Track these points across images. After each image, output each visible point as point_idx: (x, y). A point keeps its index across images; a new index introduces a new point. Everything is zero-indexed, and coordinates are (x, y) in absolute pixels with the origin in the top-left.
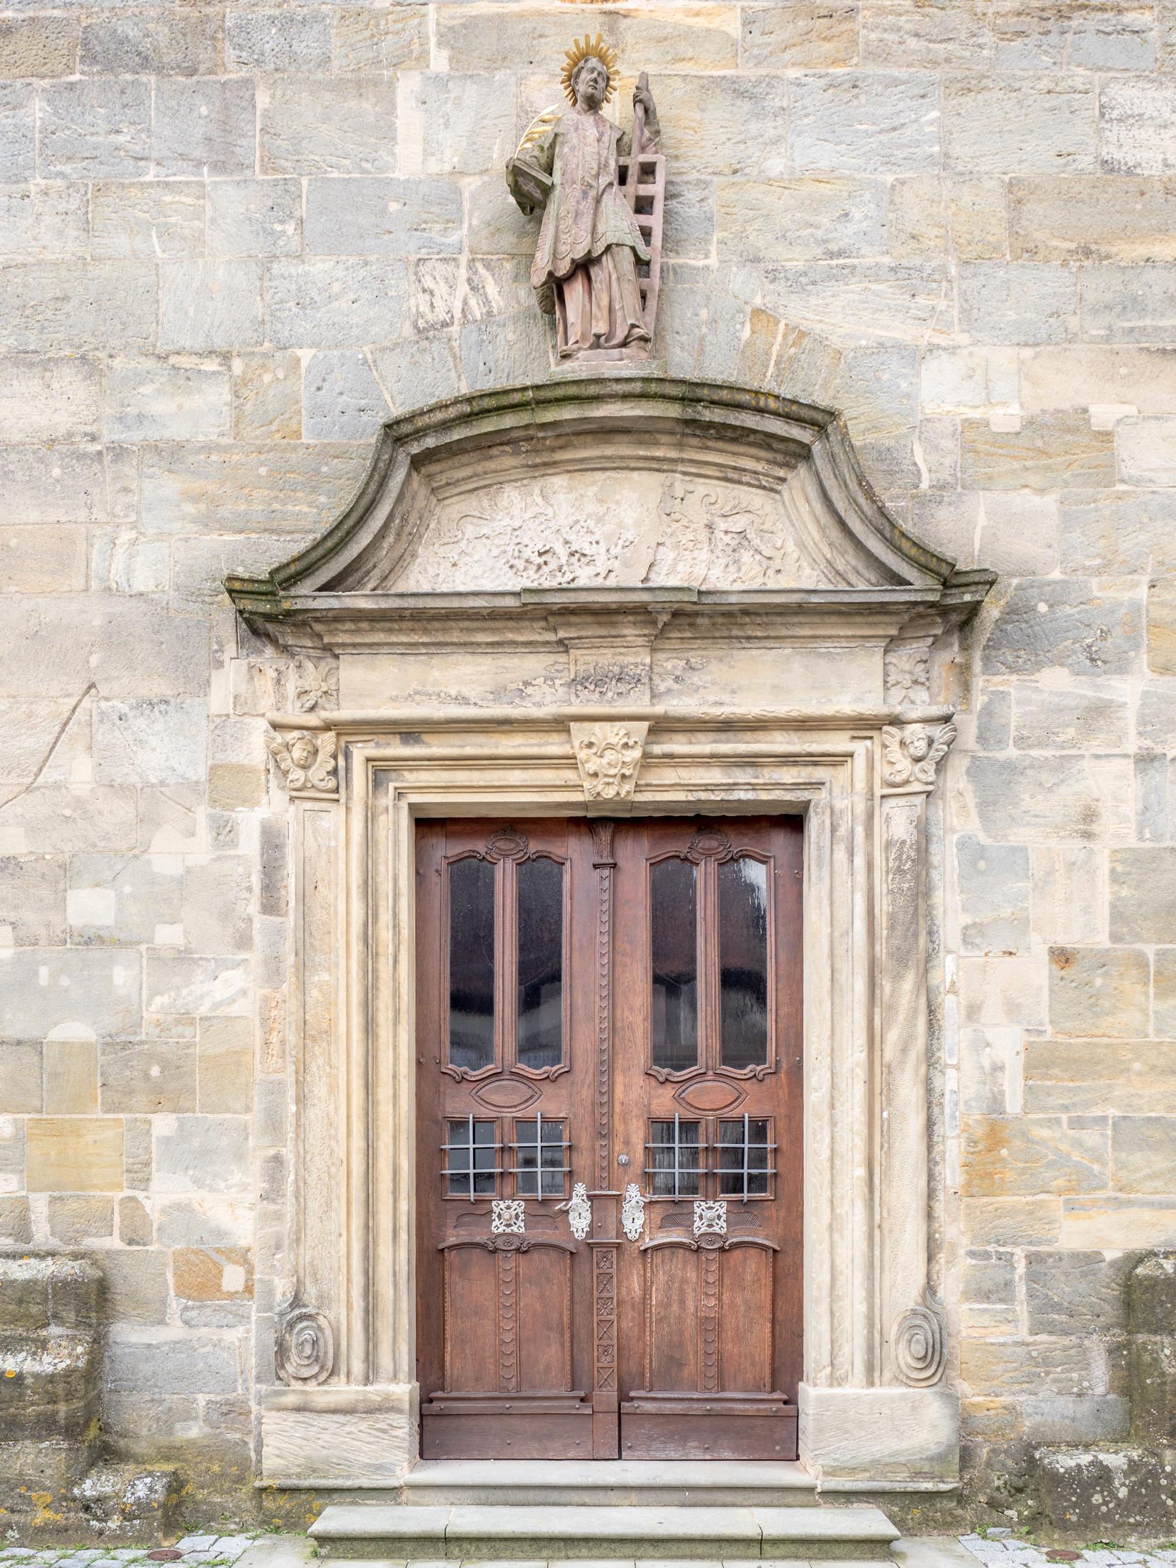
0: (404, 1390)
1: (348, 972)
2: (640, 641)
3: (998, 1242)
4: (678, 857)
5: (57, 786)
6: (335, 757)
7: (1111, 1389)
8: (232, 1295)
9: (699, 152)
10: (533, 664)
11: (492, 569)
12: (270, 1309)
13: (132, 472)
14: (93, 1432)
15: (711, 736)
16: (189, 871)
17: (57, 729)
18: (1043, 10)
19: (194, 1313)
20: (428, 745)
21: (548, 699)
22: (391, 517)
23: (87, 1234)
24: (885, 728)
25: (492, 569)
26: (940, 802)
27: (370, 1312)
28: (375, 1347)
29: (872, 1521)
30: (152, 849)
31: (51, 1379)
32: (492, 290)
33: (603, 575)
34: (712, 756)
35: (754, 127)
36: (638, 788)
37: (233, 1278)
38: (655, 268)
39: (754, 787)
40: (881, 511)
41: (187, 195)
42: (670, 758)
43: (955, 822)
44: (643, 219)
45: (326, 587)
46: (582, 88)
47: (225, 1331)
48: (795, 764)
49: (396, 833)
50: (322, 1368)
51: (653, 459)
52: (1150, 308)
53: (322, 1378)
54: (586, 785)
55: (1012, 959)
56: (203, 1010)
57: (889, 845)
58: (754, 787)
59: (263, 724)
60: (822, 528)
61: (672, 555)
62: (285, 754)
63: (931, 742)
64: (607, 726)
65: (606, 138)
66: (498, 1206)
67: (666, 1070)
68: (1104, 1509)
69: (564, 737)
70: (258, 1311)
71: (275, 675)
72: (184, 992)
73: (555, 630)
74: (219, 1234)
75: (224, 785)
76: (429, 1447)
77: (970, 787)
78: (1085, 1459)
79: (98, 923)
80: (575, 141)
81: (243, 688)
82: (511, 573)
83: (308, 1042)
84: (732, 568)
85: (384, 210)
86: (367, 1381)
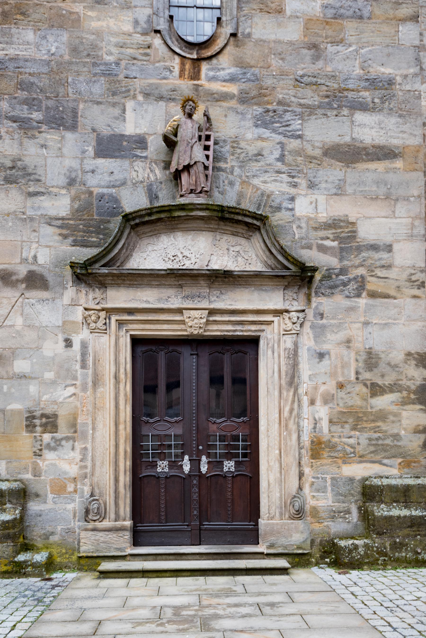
0: (128, 523)
1: (110, 388)
2: (205, 285)
3: (321, 474)
4: (218, 352)
5: (11, 326)
6: (105, 319)
7: (358, 520)
8: (70, 493)
9: (225, 131)
10: (171, 292)
11: (158, 260)
12: (82, 497)
13: (37, 225)
14: (21, 539)
15: (228, 315)
16: (56, 355)
17: (10, 308)
18: (334, 90)
19: (56, 499)
20: (137, 316)
21: (176, 302)
22: (124, 244)
23: (20, 473)
24: (284, 313)
25: (158, 260)
26: (301, 336)
27: (117, 498)
28: (118, 509)
29: (282, 563)
30: (43, 347)
31: (8, 522)
32: (157, 172)
33: (194, 263)
34: (229, 321)
35: (243, 123)
36: (205, 331)
37: (70, 488)
38: (211, 168)
39: (242, 331)
40: (282, 248)
41: (55, 136)
42: (216, 322)
43: (306, 342)
44: (207, 152)
45: (102, 266)
46: (187, 111)
47: (67, 505)
48: (255, 324)
49: (126, 344)
50: (100, 517)
51: (210, 228)
52: (368, 184)
53: (100, 520)
54: (188, 330)
55: (325, 385)
56: (61, 400)
57: (285, 349)
58: (242, 331)
59: (81, 308)
60: (264, 251)
61: (216, 258)
62: (89, 318)
63: (298, 318)
64: (195, 312)
65: (194, 127)
66: (160, 463)
67: (215, 419)
68: (356, 558)
69: (181, 315)
70: (79, 498)
71: (85, 292)
72: (54, 394)
73: (178, 282)
74: (65, 473)
75: (67, 326)
76: (136, 543)
77: (311, 332)
78: (351, 542)
79: (25, 371)
80: (184, 128)
81: (74, 296)
82: (164, 262)
83: (96, 410)
84: (235, 262)
85: (121, 145)
86: (116, 521)
